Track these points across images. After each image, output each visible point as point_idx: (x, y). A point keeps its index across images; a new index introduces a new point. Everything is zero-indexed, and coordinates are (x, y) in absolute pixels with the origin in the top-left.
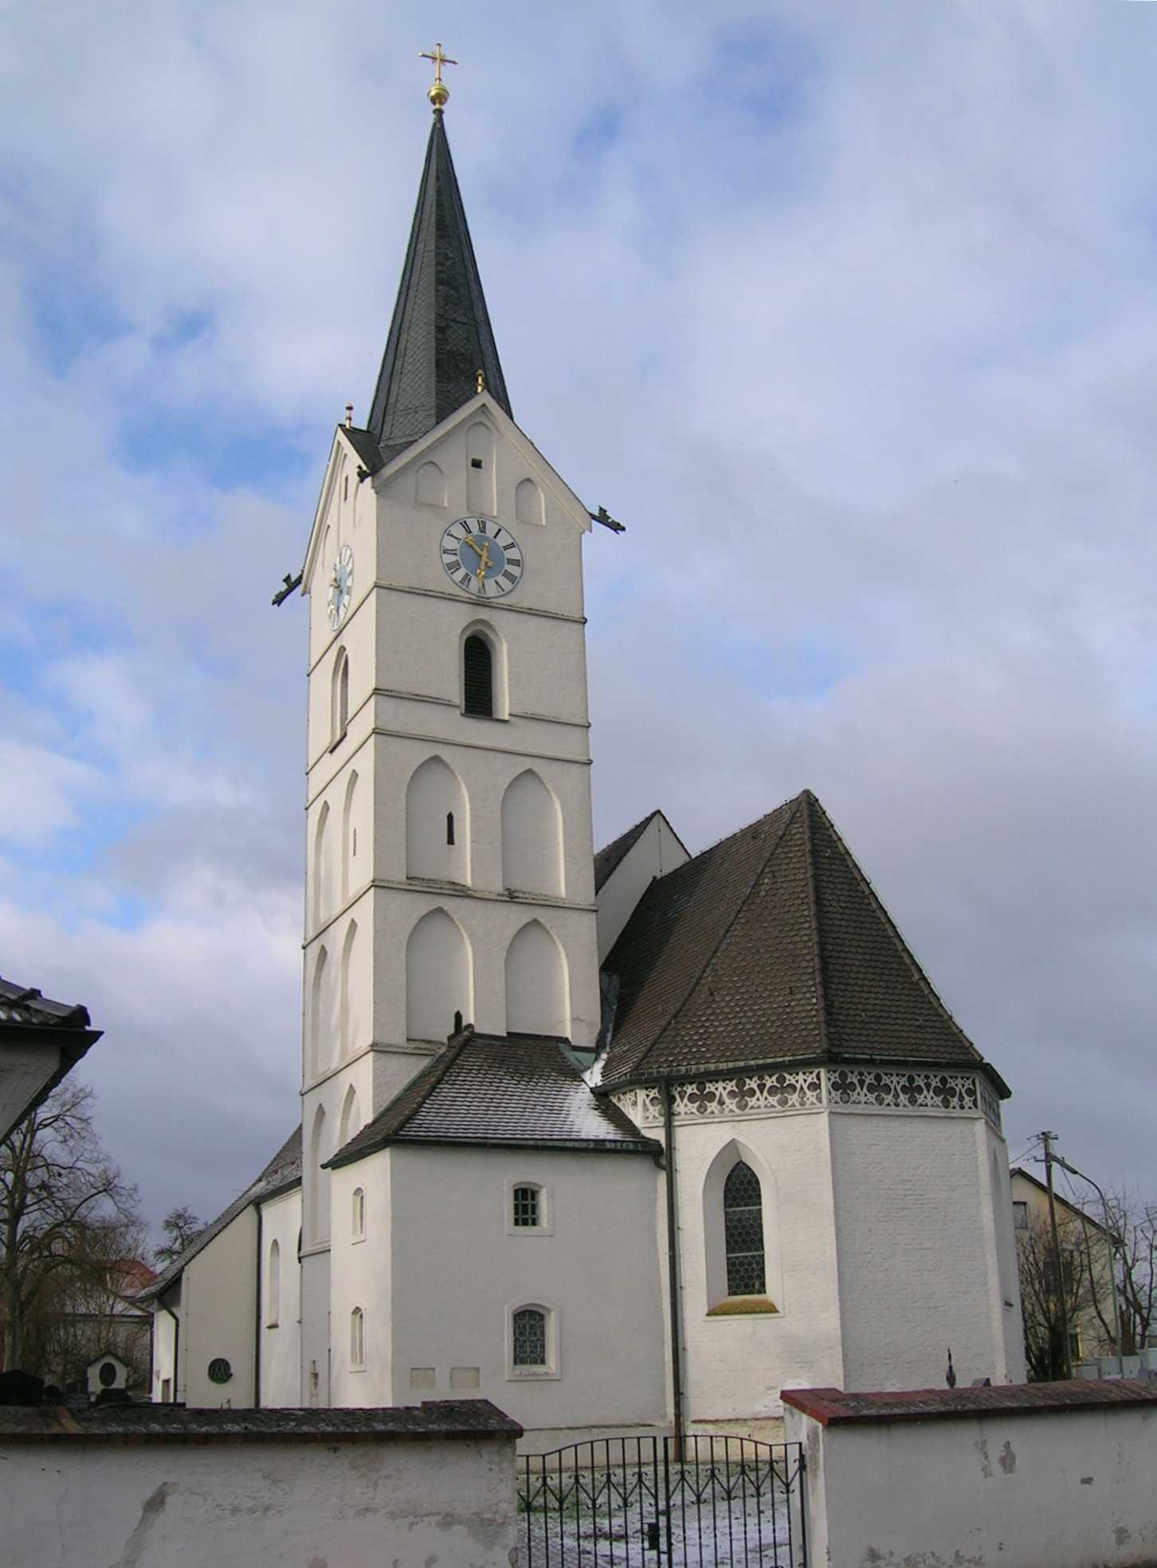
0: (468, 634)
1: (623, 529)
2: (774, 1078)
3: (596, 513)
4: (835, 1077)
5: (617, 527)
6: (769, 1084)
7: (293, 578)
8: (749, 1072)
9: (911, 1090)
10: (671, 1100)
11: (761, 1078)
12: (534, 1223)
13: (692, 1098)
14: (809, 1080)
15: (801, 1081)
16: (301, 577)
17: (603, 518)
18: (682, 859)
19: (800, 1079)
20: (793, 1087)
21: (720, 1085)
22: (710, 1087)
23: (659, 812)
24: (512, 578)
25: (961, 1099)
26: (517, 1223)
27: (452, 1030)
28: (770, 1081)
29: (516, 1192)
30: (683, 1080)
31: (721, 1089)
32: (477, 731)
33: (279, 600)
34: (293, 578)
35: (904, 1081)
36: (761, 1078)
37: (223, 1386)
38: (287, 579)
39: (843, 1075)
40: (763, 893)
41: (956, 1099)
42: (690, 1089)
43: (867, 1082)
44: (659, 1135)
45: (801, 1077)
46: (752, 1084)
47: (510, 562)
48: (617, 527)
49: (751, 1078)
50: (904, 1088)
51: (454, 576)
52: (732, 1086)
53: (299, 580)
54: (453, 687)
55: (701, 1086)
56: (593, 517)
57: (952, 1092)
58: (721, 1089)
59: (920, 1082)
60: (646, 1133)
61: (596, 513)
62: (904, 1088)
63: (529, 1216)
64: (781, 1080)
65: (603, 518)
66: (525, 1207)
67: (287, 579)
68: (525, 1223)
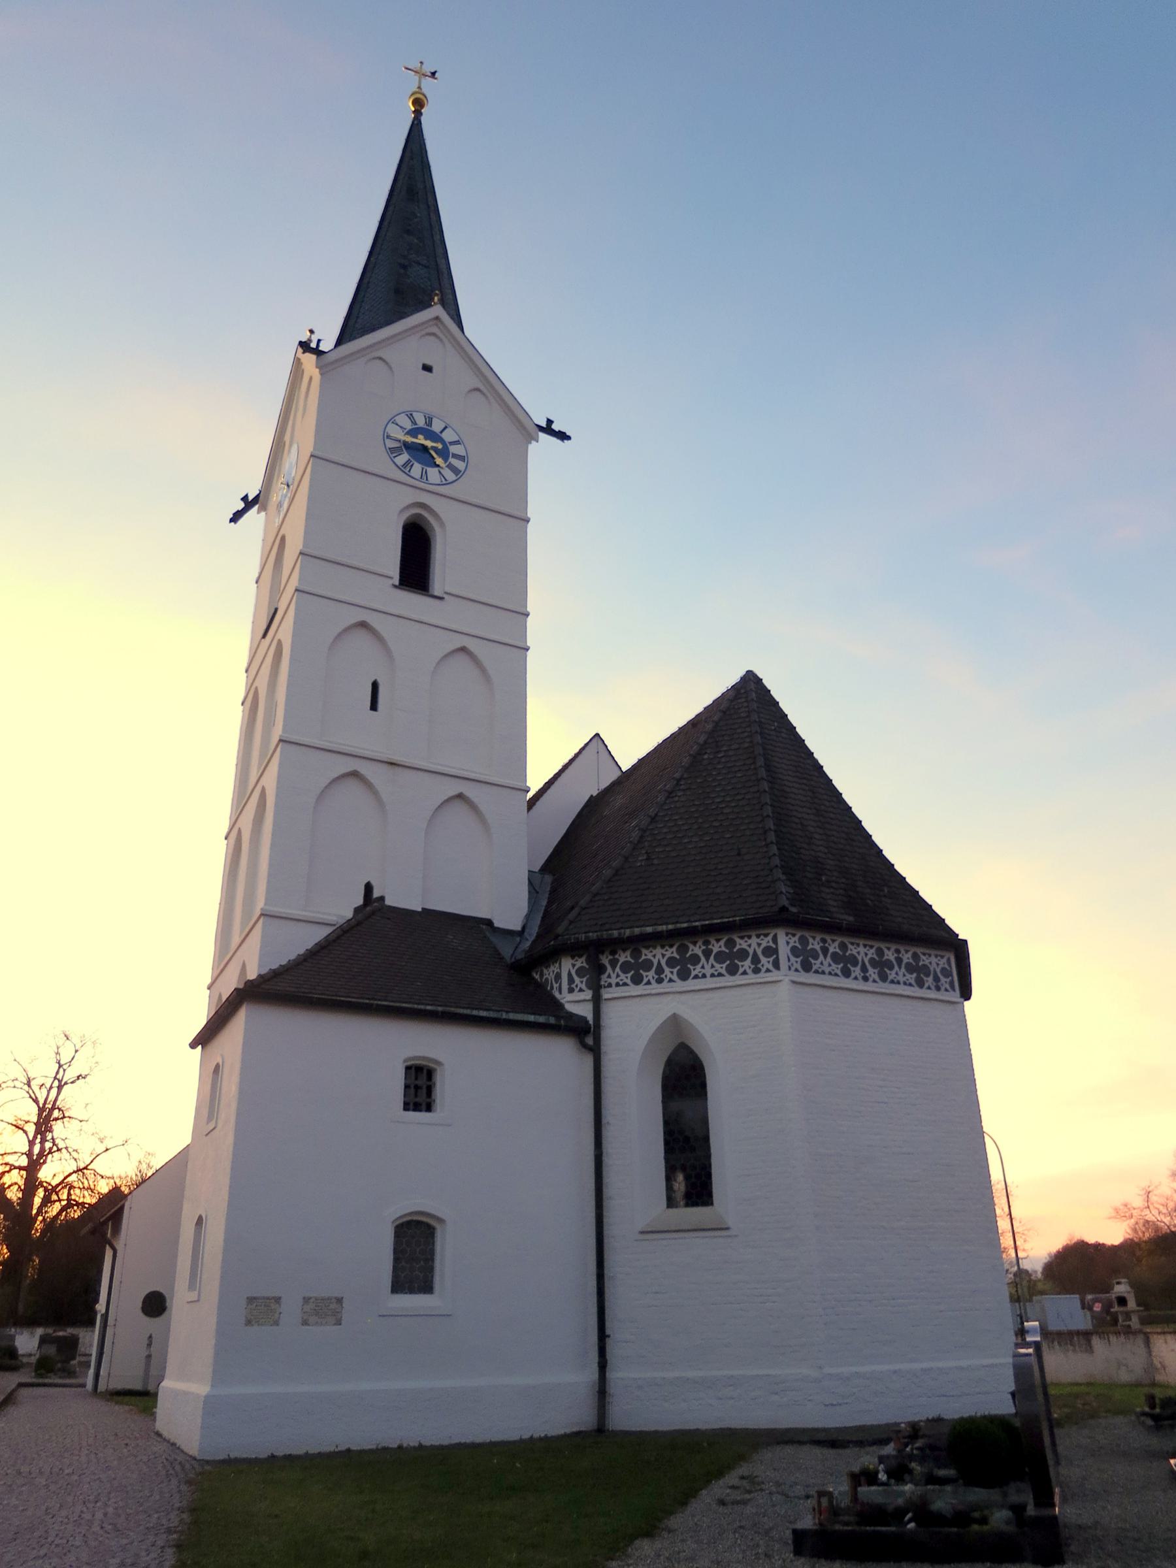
0: (406, 516)
1: (569, 438)
2: (722, 943)
3: (544, 424)
4: (794, 941)
5: (563, 436)
6: (715, 950)
7: (250, 498)
8: (692, 933)
9: (883, 966)
10: (601, 969)
11: (707, 943)
12: (429, 1108)
13: (625, 968)
14: (764, 944)
15: (754, 945)
16: (258, 496)
17: (548, 428)
18: (614, 776)
19: (753, 943)
20: (743, 954)
21: (658, 951)
22: (646, 954)
23: (597, 735)
24: (456, 471)
25: (937, 979)
26: (406, 1107)
27: (360, 901)
28: (717, 947)
29: (408, 1068)
30: (614, 945)
31: (658, 955)
32: (411, 602)
33: (236, 517)
34: (250, 498)
35: (872, 953)
36: (707, 943)
37: (141, 1314)
38: (245, 499)
39: (804, 941)
40: (705, 762)
41: (930, 979)
42: (624, 957)
43: (831, 950)
44: (585, 1011)
45: (754, 941)
46: (697, 950)
47: (455, 456)
48: (563, 436)
49: (695, 943)
50: (872, 961)
51: (396, 460)
52: (672, 952)
53: (256, 500)
54: (392, 563)
55: (636, 953)
56: (541, 428)
57: (925, 970)
58: (659, 956)
59: (890, 955)
60: (570, 1008)
61: (544, 424)
62: (872, 961)
63: (422, 1098)
64: (731, 943)
65: (548, 429)
66: (420, 1087)
67: (245, 499)
68: (417, 1107)
